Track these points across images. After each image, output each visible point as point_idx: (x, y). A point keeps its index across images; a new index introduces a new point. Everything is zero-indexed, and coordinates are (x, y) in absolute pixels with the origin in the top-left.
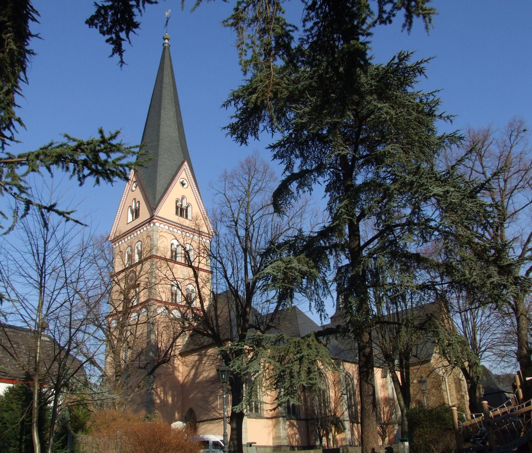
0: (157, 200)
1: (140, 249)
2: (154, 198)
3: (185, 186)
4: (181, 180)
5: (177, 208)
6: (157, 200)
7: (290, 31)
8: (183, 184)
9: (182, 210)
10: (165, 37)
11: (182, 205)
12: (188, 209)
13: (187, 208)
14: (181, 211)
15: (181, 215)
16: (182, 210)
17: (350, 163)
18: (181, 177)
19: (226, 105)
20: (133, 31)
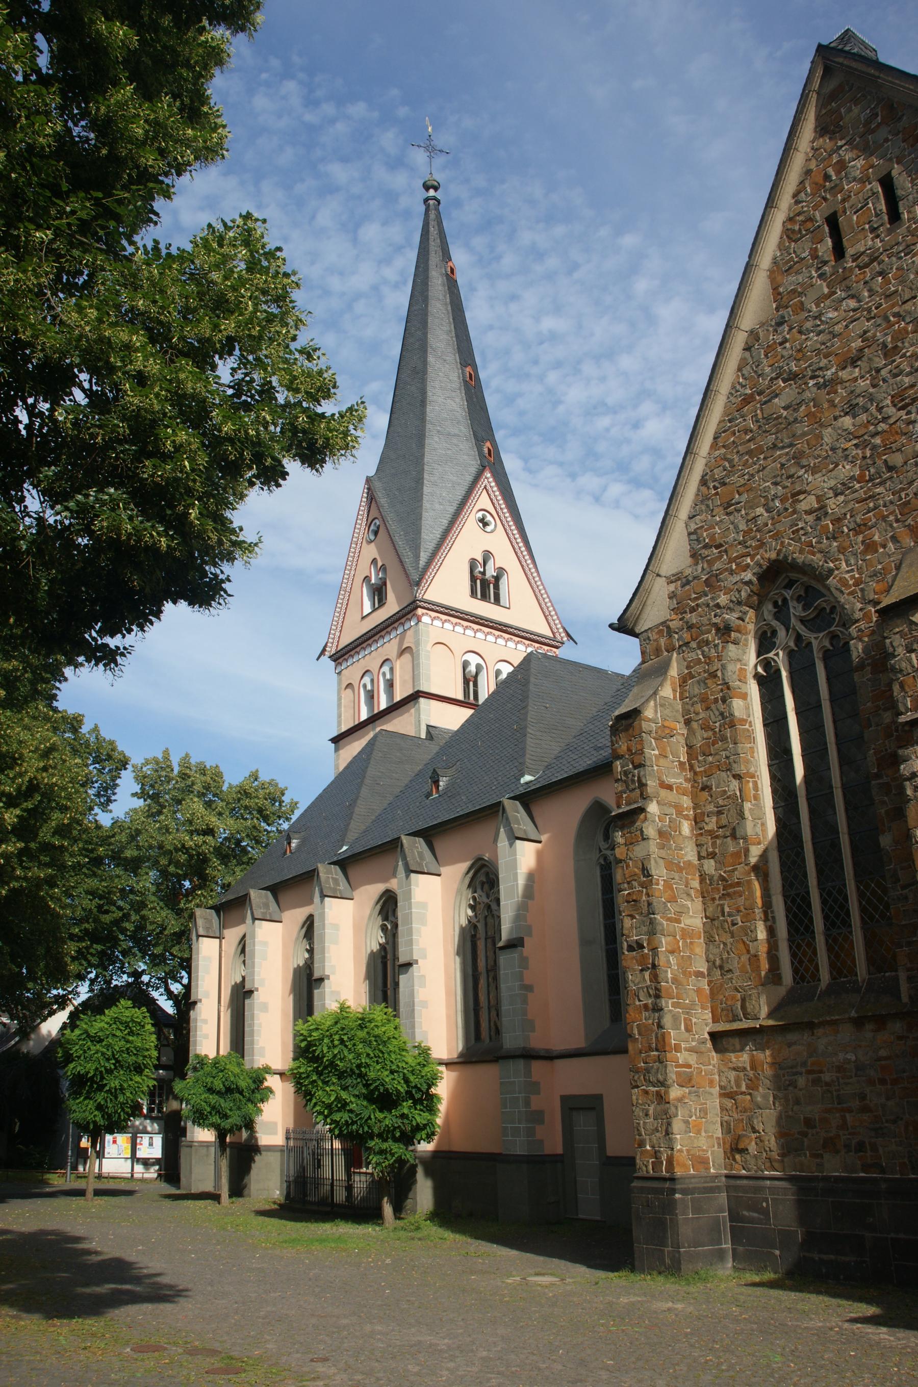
0: (424, 557)
1: (388, 677)
2: (416, 548)
3: (488, 529)
4: (480, 515)
5: (473, 579)
6: (424, 557)
7: (38, 884)
8: (484, 523)
9: (485, 584)
10: (429, 183)
11: (484, 573)
12: (479, 678)
13: (477, 674)
14: (485, 585)
15: (485, 597)
16: (485, 584)
17: (184, 16)
18: (477, 507)
19: (115, 800)
20: (635, 624)
